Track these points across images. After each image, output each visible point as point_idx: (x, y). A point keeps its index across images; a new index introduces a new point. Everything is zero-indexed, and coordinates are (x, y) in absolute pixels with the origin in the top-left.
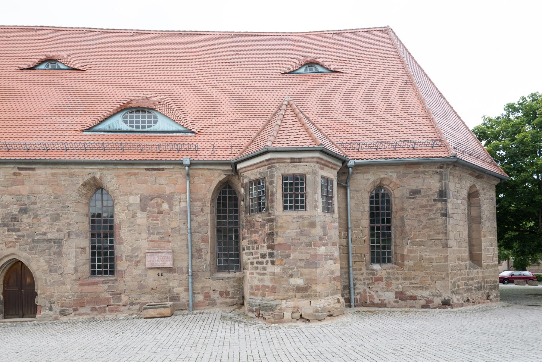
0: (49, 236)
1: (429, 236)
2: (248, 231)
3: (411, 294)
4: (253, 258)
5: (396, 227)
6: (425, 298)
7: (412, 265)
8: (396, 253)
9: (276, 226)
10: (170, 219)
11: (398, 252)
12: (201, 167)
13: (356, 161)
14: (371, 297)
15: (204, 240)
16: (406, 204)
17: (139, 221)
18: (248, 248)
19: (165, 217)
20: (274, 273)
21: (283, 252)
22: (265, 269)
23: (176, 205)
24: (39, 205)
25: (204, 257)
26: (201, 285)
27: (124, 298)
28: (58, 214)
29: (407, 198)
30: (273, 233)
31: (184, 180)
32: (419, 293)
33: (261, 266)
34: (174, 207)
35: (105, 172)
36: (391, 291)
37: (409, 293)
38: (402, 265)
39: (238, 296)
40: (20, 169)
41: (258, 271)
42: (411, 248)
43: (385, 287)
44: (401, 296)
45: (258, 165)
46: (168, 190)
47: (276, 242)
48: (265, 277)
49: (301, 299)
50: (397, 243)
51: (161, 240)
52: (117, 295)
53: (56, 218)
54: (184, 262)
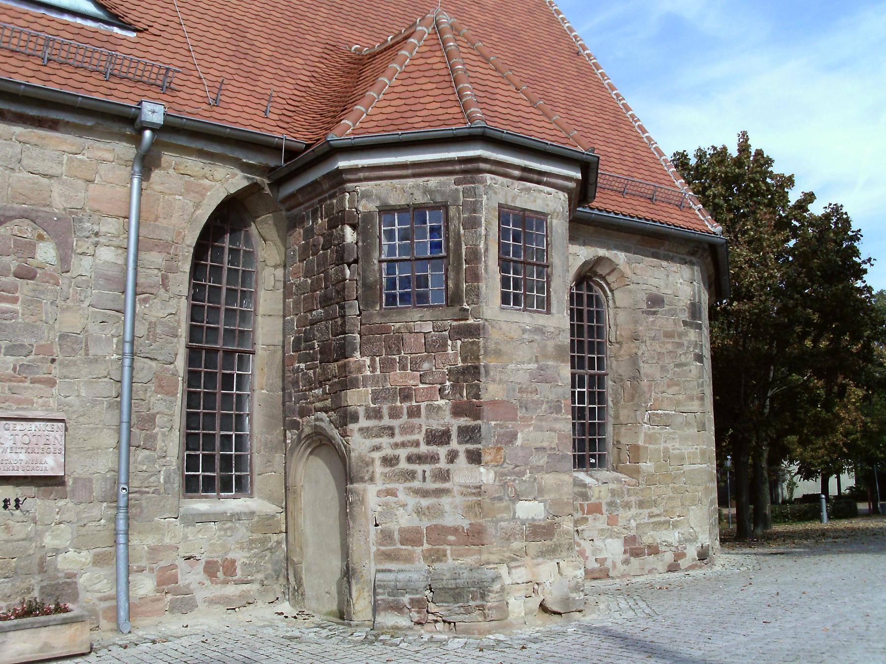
1: (678, 403)
2: (373, 361)
3: (650, 541)
4: (396, 445)
5: (619, 380)
6: (673, 548)
7: (652, 470)
8: (618, 442)
9: (485, 347)
10: (59, 302)
11: (624, 441)
15: (164, 387)
16: (641, 325)
18: (376, 414)
19: (42, 292)
20: (480, 487)
21: (501, 426)
22: (444, 476)
23: (83, 254)
25: (159, 444)
26: (151, 540)
29: (643, 312)
30: (477, 368)
31: (125, 172)
33: (427, 467)
34: (74, 260)
37: (647, 539)
38: (634, 473)
39: (260, 576)
41: (416, 484)
42: (652, 431)
43: (605, 526)
45: (417, 171)
47: (485, 397)
48: (445, 501)
49: (540, 560)
50: (623, 419)
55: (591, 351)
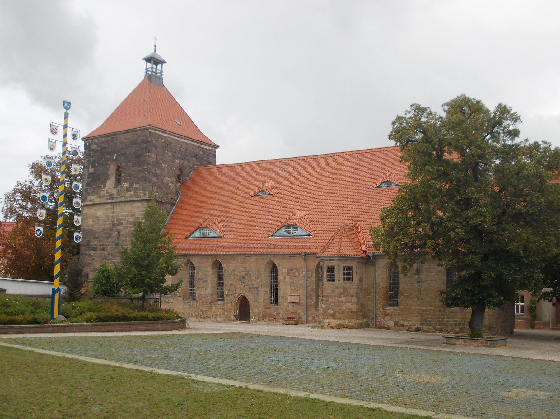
0: (255, 286)
12: (310, 256)
14: (384, 324)
15: (312, 290)
24: (251, 272)
27: (281, 316)
28: (258, 276)
32: (406, 323)
35: (275, 258)
36: (393, 321)
37: (401, 323)
40: (245, 257)
44: (397, 324)
46: (298, 266)
52: (278, 314)
53: (257, 278)
54: (303, 301)
55: (192, 281)
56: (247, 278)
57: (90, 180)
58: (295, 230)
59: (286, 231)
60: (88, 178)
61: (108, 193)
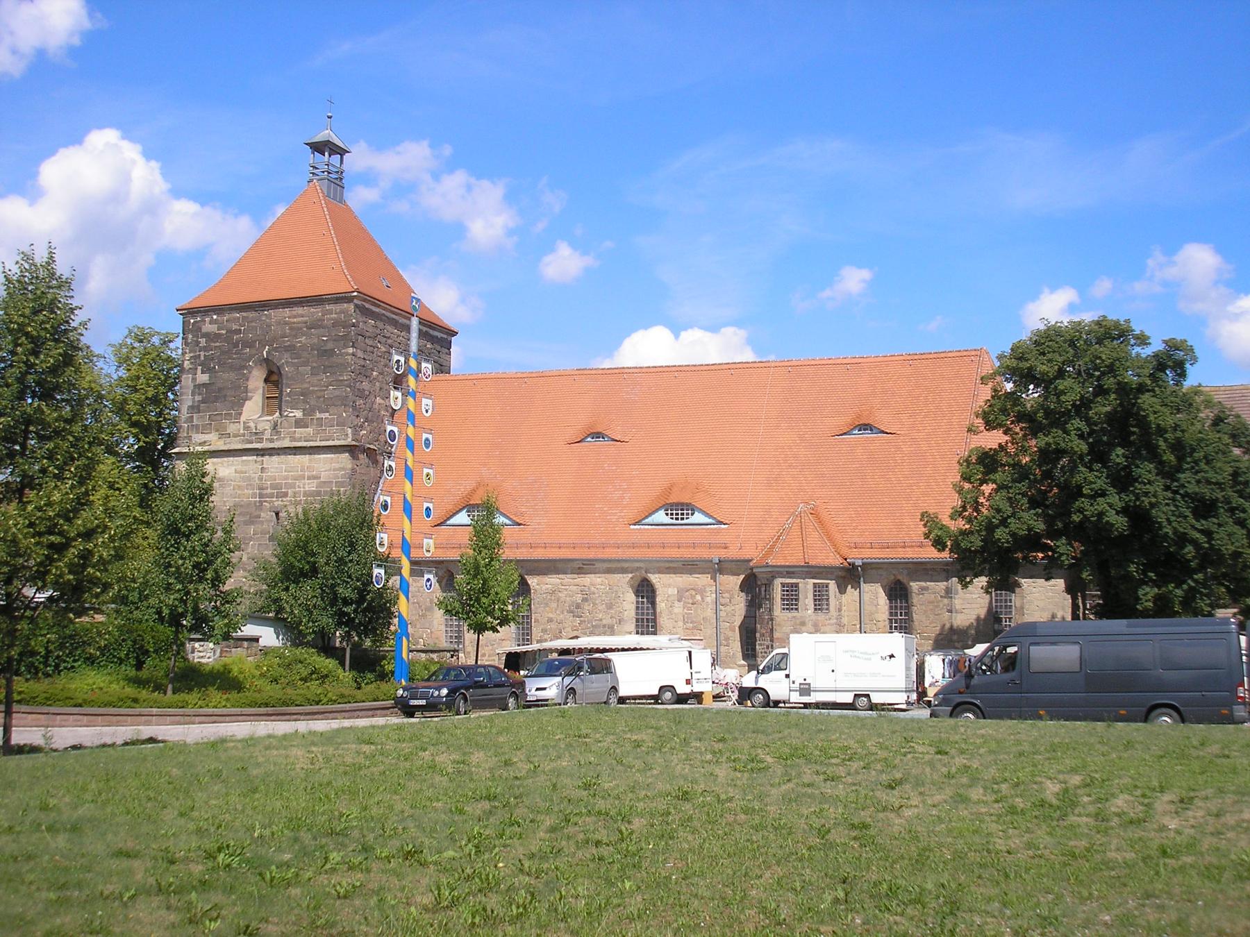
0: (604, 622)
13: (865, 560)
17: (676, 610)
40: (583, 564)
51: (694, 628)
56: (586, 607)
57: (198, 398)
58: (688, 514)
59: (667, 514)
60: (193, 394)
61: (247, 428)
